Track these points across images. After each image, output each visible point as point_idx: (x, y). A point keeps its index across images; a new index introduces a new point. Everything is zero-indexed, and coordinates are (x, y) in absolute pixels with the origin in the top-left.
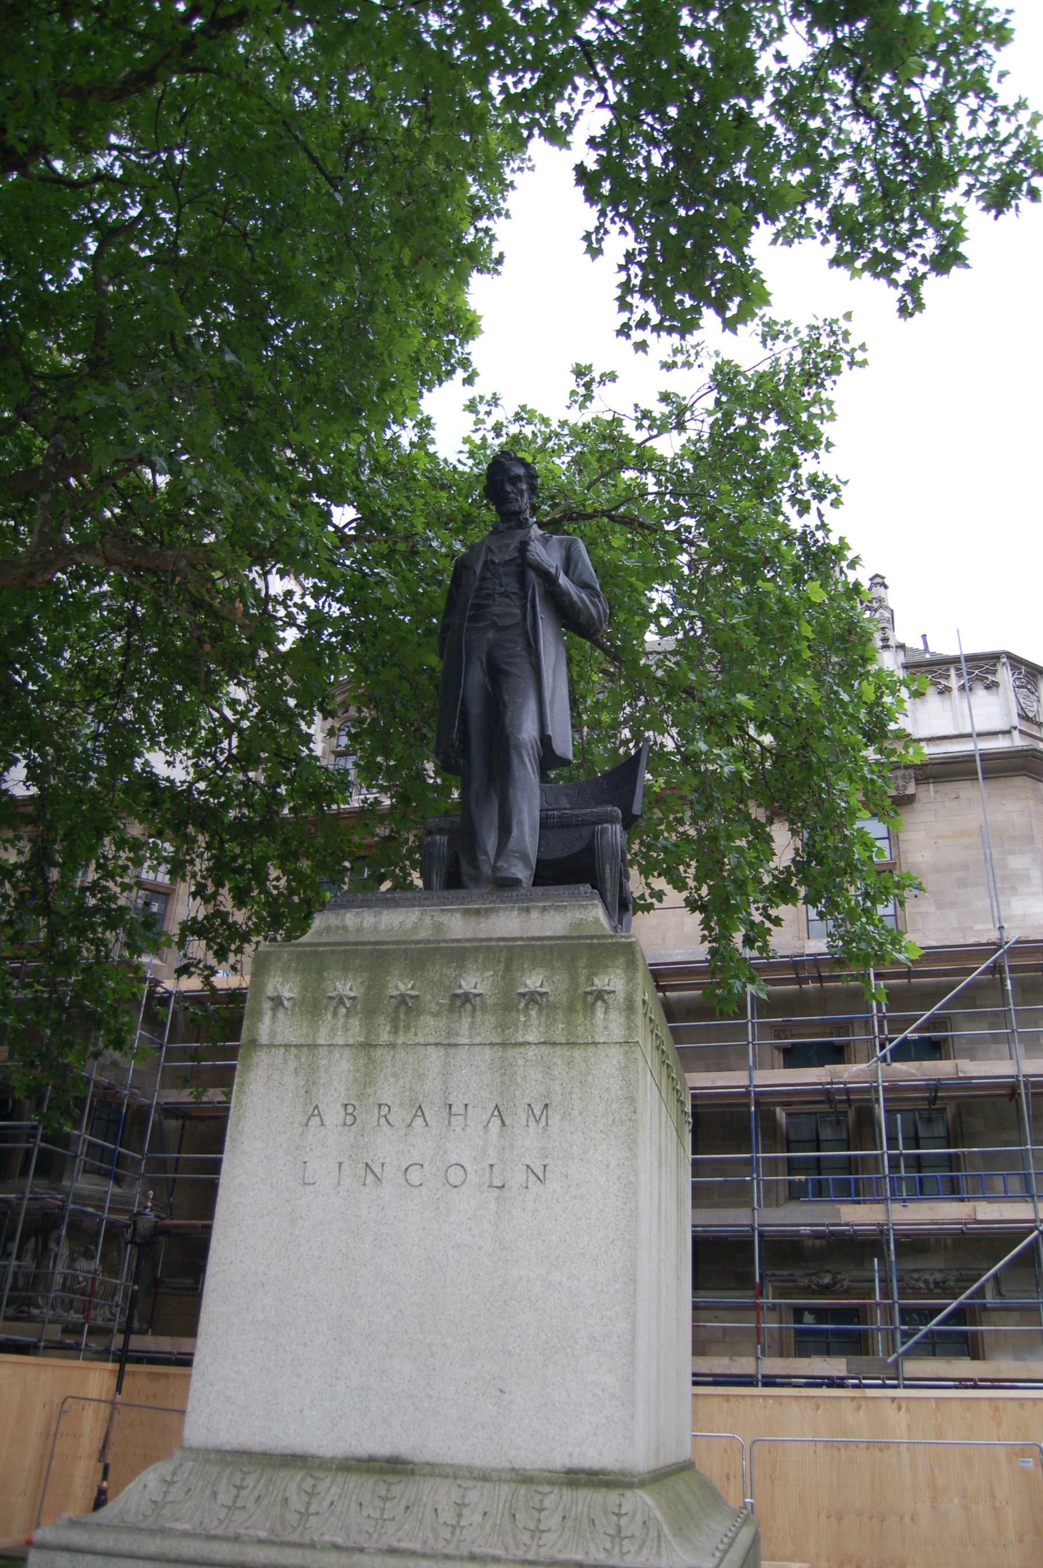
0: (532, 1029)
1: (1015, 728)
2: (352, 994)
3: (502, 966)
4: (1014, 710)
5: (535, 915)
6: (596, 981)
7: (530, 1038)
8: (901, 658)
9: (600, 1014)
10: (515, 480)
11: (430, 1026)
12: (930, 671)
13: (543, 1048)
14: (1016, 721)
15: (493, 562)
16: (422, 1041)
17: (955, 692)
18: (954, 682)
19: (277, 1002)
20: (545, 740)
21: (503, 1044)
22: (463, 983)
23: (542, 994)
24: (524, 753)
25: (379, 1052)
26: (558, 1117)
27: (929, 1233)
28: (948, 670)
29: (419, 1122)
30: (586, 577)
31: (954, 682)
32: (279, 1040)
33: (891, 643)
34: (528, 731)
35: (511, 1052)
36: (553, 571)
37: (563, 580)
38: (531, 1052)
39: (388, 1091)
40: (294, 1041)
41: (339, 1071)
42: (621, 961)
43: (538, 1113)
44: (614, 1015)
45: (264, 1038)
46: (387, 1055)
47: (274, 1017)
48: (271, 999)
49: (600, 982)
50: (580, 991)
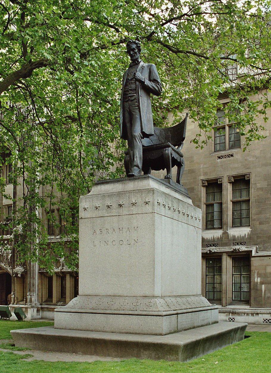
10: (133, 50)
15: (128, 79)
19: (85, 209)
23: (135, 203)
24: (136, 138)
30: (155, 78)
36: (143, 80)
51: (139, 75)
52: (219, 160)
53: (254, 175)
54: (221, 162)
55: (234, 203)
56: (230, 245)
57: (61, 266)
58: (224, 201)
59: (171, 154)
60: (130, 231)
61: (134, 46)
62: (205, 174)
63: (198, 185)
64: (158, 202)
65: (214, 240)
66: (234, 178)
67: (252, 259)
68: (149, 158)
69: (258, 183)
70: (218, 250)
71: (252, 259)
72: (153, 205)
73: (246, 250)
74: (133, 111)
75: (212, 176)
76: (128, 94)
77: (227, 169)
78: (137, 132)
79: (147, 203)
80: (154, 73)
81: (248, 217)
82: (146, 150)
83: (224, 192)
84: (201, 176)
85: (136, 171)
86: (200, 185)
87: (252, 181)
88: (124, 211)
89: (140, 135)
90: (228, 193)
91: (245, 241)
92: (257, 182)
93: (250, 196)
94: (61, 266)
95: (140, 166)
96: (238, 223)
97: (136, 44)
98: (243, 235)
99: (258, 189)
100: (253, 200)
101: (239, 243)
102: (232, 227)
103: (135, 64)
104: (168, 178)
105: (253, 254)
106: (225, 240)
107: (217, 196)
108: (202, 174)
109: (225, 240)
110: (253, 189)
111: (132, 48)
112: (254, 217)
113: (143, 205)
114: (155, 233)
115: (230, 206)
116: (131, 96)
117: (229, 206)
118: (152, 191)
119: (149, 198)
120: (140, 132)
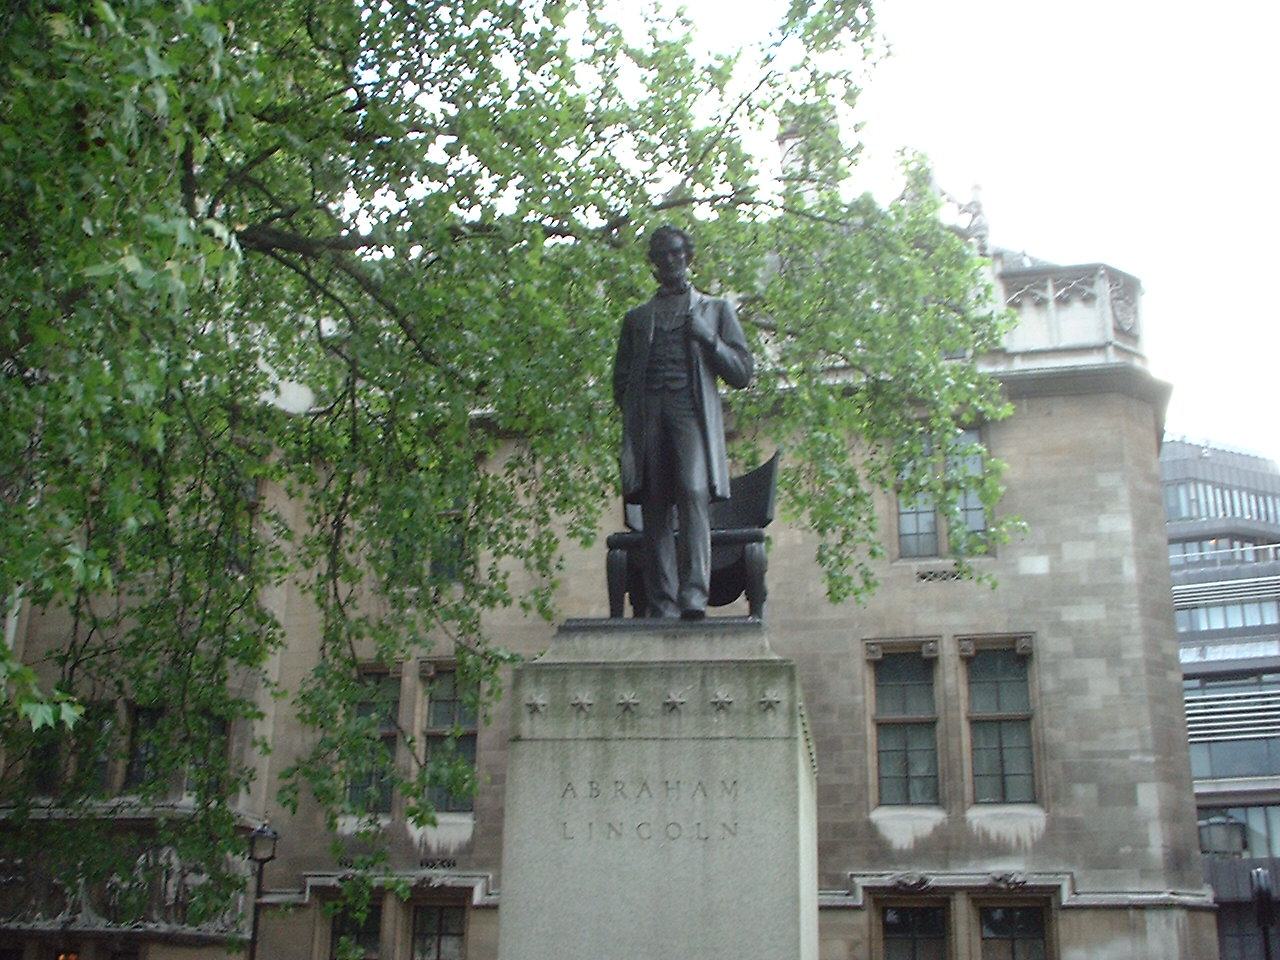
0: (721, 724)
1: (1110, 343)
3: (698, 682)
4: (1110, 323)
5: (717, 640)
6: (768, 693)
7: (722, 734)
8: (999, 268)
10: (675, 252)
11: (651, 725)
12: (1026, 284)
13: (731, 741)
14: (1111, 336)
15: (661, 329)
16: (643, 736)
17: (1052, 305)
18: (1050, 294)
20: (712, 488)
21: (703, 739)
22: (672, 694)
25: (612, 744)
27: (1102, 370)
28: (1045, 280)
30: (735, 338)
31: (1050, 294)
33: (989, 251)
34: (699, 484)
36: (710, 339)
37: (721, 347)
38: (722, 744)
39: (620, 772)
40: (549, 736)
41: (585, 757)
42: (784, 679)
46: (620, 745)
50: (756, 700)
57: (68, 910)
60: (709, 793)
65: (443, 851)
66: (976, 645)
71: (1061, 915)
74: (681, 423)
76: (664, 371)
77: (945, 617)
79: (722, 707)
88: (688, 725)
94: (68, 910)
113: (755, 712)
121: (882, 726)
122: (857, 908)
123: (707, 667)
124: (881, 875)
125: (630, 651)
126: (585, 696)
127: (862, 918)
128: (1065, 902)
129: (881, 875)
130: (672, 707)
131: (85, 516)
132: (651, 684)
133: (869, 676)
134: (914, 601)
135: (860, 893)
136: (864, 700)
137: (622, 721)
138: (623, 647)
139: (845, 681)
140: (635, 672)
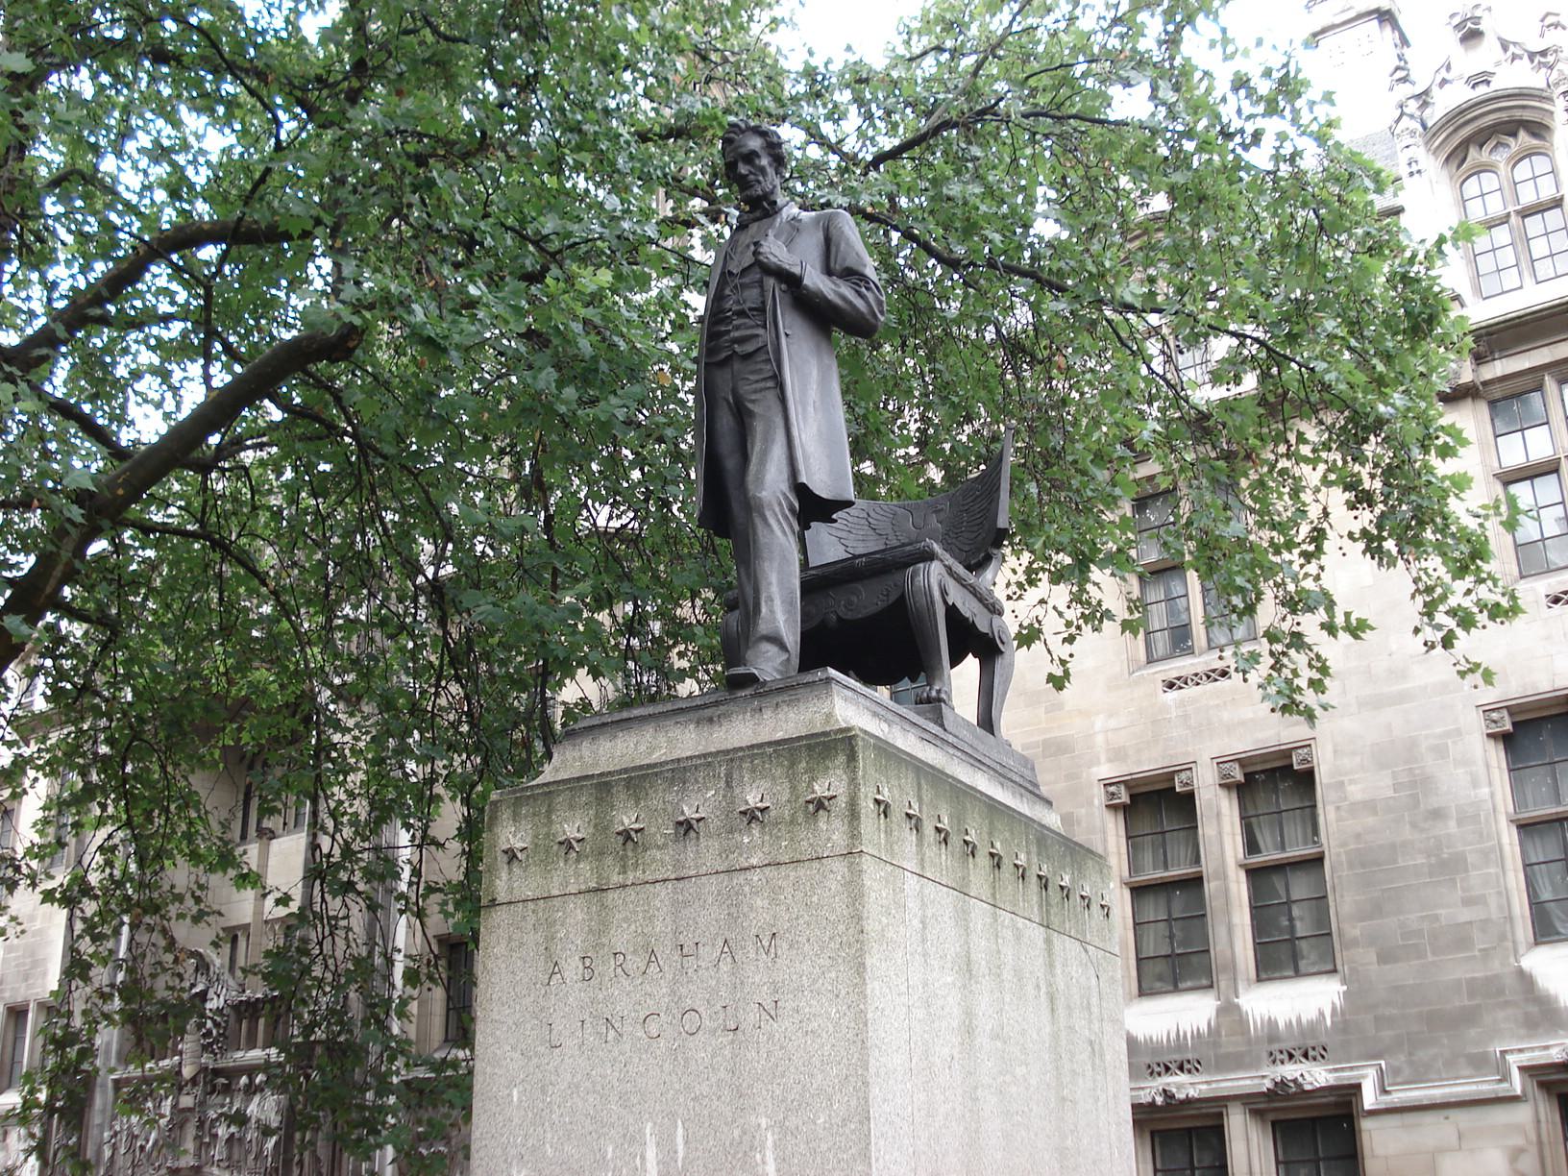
2: (579, 836)
3: (722, 784)
5: (768, 714)
7: (754, 861)
9: (822, 825)
10: (750, 157)
11: (661, 860)
19: (511, 855)
23: (763, 810)
24: (768, 514)
25: (611, 895)
26: (785, 946)
29: (653, 968)
30: (850, 262)
32: (517, 895)
35: (739, 879)
36: (797, 270)
38: (755, 876)
39: (621, 938)
43: (766, 944)
44: (837, 823)
45: (502, 897)
47: (510, 871)
48: (505, 852)
49: (820, 789)
51: (776, 250)
52: (1173, 694)
53: (1329, 748)
54: (1181, 704)
55: (1254, 873)
56: (1255, 1064)
58: (1208, 866)
59: (944, 593)
61: (755, 143)
62: (1117, 755)
63: (1091, 803)
64: (877, 802)
65: (1180, 1043)
66: (1242, 766)
67: (1366, 1125)
68: (839, 618)
69: (1351, 782)
70: (1204, 1087)
72: (853, 814)
73: (1332, 1082)
74: (753, 401)
75: (1147, 763)
76: (728, 332)
78: (770, 484)
80: (848, 243)
81: (1324, 935)
82: (817, 584)
83: (1206, 829)
84: (1099, 763)
85: (767, 664)
86: (1096, 802)
87: (1323, 777)
88: (706, 852)
89: (787, 498)
90: (1221, 825)
91: (1323, 1040)
92: (1346, 779)
93: (1324, 840)
95: (792, 638)
96: (1278, 957)
97: (764, 134)
98: (1309, 1014)
99: (1356, 808)
100: (1338, 855)
101: (1297, 1054)
102: (1259, 980)
103: (758, 214)
104: (929, 700)
105: (1369, 1099)
106: (1230, 1045)
107: (1178, 850)
108: (1103, 758)
109: (1229, 1042)
110: (1330, 809)
111: (744, 150)
112: (1354, 931)
114: (868, 962)
115: (1239, 888)
116: (741, 340)
117: (1233, 887)
118: (840, 745)
119: (831, 783)
120: (785, 486)
121: (1526, 828)
122: (1513, 1099)
123: (732, 758)
124: (1547, 1048)
125: (652, 749)
126: (572, 826)
127: (1522, 1114)
128: (1367, 1107)
129: (1547, 1048)
130: (686, 827)
131: (434, 715)
132: (660, 797)
133: (1497, 755)
134: (1548, 638)
135: (1516, 1075)
136: (1492, 795)
137: (623, 858)
138: (642, 748)
139: (1461, 771)
140: (638, 780)
